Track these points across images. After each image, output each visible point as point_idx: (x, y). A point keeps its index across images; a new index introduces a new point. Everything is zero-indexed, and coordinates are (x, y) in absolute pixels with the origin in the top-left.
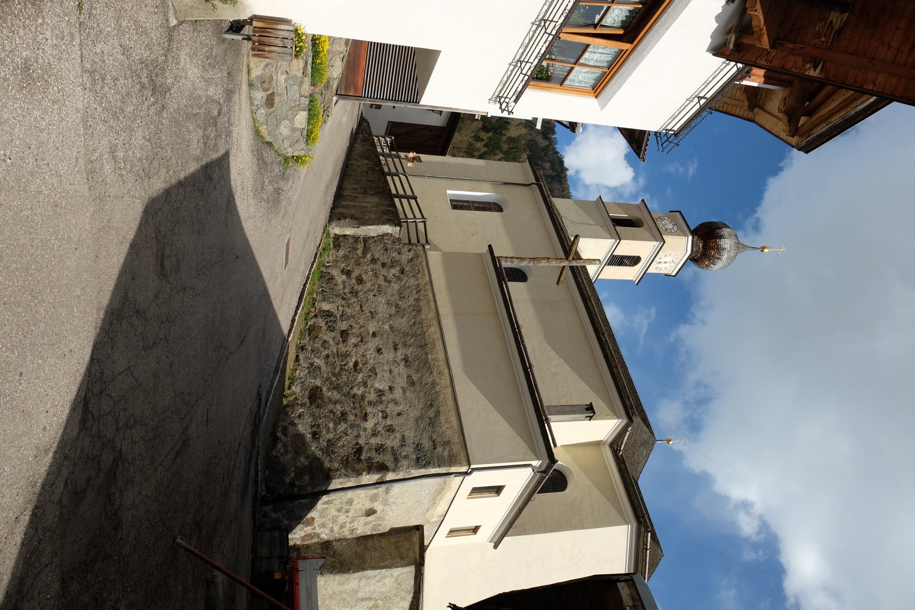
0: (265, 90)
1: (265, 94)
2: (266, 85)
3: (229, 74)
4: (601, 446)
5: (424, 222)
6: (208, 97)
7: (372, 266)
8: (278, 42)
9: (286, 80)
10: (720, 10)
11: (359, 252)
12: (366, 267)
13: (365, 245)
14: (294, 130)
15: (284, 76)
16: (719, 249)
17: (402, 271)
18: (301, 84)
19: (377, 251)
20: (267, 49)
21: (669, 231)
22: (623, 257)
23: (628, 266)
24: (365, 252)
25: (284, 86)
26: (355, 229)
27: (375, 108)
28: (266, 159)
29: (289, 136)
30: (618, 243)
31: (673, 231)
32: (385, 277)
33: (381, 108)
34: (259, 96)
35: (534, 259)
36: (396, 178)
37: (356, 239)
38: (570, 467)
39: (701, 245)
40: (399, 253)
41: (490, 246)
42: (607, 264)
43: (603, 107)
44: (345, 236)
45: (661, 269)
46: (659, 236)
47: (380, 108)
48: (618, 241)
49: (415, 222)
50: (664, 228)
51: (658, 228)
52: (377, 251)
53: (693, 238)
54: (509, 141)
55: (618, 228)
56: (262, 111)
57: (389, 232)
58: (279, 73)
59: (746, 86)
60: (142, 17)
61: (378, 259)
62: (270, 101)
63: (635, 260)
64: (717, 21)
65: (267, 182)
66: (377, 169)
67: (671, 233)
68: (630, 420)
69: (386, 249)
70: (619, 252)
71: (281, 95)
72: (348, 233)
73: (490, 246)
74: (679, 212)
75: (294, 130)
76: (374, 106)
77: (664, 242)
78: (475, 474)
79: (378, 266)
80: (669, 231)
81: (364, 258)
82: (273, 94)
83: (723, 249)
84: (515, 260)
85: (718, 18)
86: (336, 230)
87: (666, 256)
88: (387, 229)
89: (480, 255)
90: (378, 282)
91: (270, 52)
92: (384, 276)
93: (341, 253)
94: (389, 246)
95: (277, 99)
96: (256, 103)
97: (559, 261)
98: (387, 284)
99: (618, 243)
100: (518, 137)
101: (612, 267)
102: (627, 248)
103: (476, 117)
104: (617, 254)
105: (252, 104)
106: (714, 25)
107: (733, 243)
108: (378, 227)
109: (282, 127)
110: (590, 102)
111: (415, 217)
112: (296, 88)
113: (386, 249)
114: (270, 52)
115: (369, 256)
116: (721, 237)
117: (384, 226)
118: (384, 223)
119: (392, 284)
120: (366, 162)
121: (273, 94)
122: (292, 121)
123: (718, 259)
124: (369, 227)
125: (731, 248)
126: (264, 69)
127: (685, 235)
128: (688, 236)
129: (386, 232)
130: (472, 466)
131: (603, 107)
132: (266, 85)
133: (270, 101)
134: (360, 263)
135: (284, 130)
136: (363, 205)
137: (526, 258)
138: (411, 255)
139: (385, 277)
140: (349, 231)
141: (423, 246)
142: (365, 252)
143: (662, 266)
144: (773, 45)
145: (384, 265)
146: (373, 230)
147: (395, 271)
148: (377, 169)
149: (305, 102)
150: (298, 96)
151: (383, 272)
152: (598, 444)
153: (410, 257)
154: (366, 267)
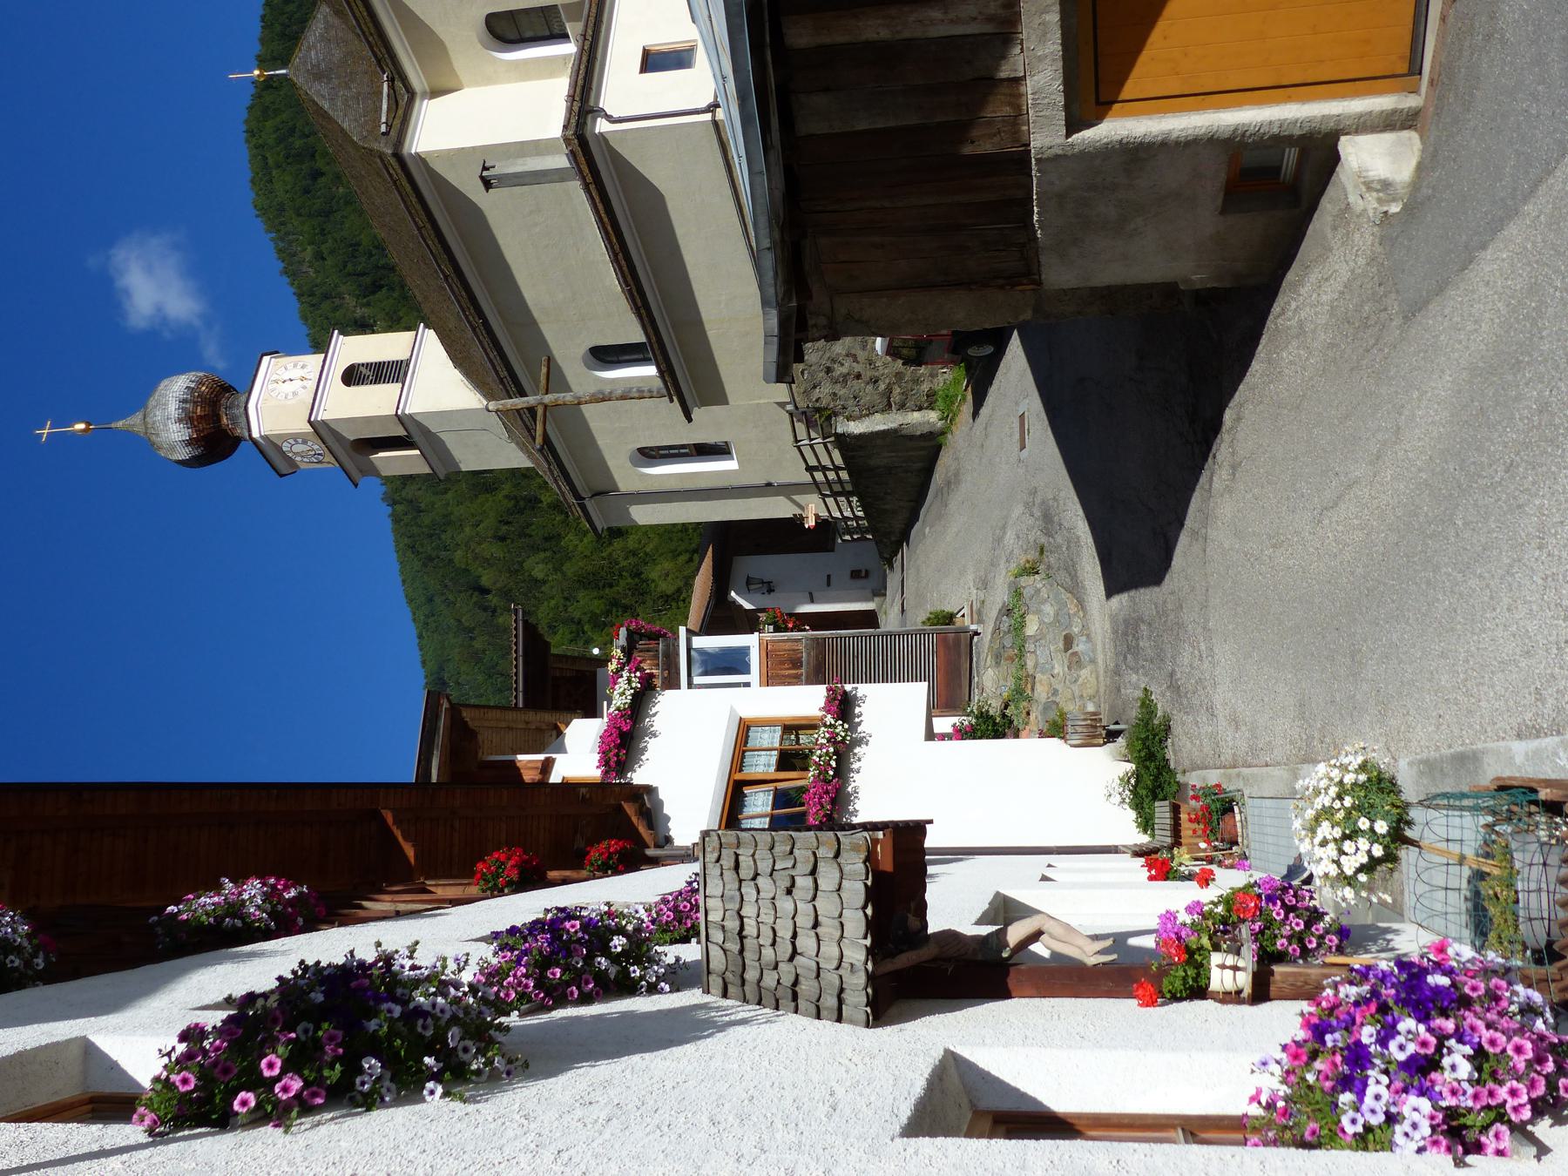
0: (1075, 654)
1: (1075, 649)
2: (1075, 659)
3: (1119, 690)
4: (428, 90)
5: (797, 441)
6: (1137, 673)
7: (876, 374)
8: (1079, 729)
9: (1053, 668)
10: (670, 825)
11: (897, 390)
12: (886, 371)
13: (889, 401)
14: (1038, 612)
15: (1056, 671)
16: (188, 419)
17: (829, 370)
18: (1035, 667)
19: (869, 394)
20: (1089, 722)
21: (300, 441)
22: (377, 381)
23: (363, 365)
24: (889, 391)
25: (1055, 661)
26: (905, 422)
27: (860, 571)
28: (1067, 575)
29: (1043, 603)
30: (398, 408)
31: (292, 441)
32: (856, 360)
33: (849, 573)
34: (1080, 647)
35: (603, 400)
36: (813, 462)
37: (902, 407)
38: (479, 46)
39: (225, 420)
40: (835, 394)
41: (690, 420)
42: (404, 365)
43: (732, 710)
44: (920, 409)
45: (295, 366)
46: (322, 430)
47: (852, 572)
48: (399, 412)
49: (811, 440)
50: (310, 443)
51: (324, 443)
52: (869, 394)
53: (250, 435)
54: (496, 485)
55: (401, 432)
56: (1076, 630)
57: (852, 424)
58: (1061, 674)
59: (540, 753)
60: (1189, 744)
61: (868, 383)
62: (1068, 641)
63: (352, 376)
64: (666, 815)
65: (1064, 549)
66: (870, 500)
67: (295, 437)
68: (398, 156)
69: (855, 398)
70: (391, 389)
71: (1056, 651)
72: (916, 414)
73: (690, 420)
74: (282, 476)
75: (1038, 612)
76: (863, 574)
77: (309, 421)
78: (703, 104)
79: (867, 374)
80: (300, 441)
81: (889, 383)
82: (1066, 650)
83: (180, 421)
84: (636, 395)
85: (668, 819)
86: (932, 416)
87: (295, 394)
88: (856, 428)
89: (705, 402)
90: (866, 353)
91: (1085, 720)
92: (858, 362)
93: (925, 387)
94: (851, 402)
95: (1061, 645)
96: (1084, 638)
97: (559, 402)
98: (853, 352)
99: (398, 408)
100: (476, 496)
101: (395, 359)
102: (375, 402)
103: (771, 628)
104: (390, 385)
105: (1088, 636)
106: (666, 811)
107: (163, 434)
108: (870, 430)
109: (1052, 613)
110: (749, 713)
111: (812, 446)
112: (1041, 661)
113: (855, 398)
114: (1085, 720)
115: (882, 387)
116: (189, 442)
117: (862, 431)
118: (861, 436)
119: (844, 353)
120: (887, 507)
121: (1066, 650)
122: (1041, 622)
123: (184, 401)
124: (885, 427)
125: (165, 425)
126: (1079, 676)
127: (266, 438)
128: (261, 436)
129: (857, 422)
130: (708, 117)
131: (732, 710)
132: (1075, 659)
133: (1068, 641)
134: (895, 376)
135: (1049, 610)
136: (893, 454)
137: (617, 399)
138: (816, 393)
139: (856, 360)
140: (915, 417)
141: (796, 408)
142: (889, 391)
143: (296, 373)
144: (620, 809)
145: (858, 376)
146: (878, 423)
147: (839, 370)
148: (870, 500)
149: (1030, 647)
150: (1038, 652)
151: (857, 368)
152: (435, 93)
153: (817, 390)
154: (886, 371)
